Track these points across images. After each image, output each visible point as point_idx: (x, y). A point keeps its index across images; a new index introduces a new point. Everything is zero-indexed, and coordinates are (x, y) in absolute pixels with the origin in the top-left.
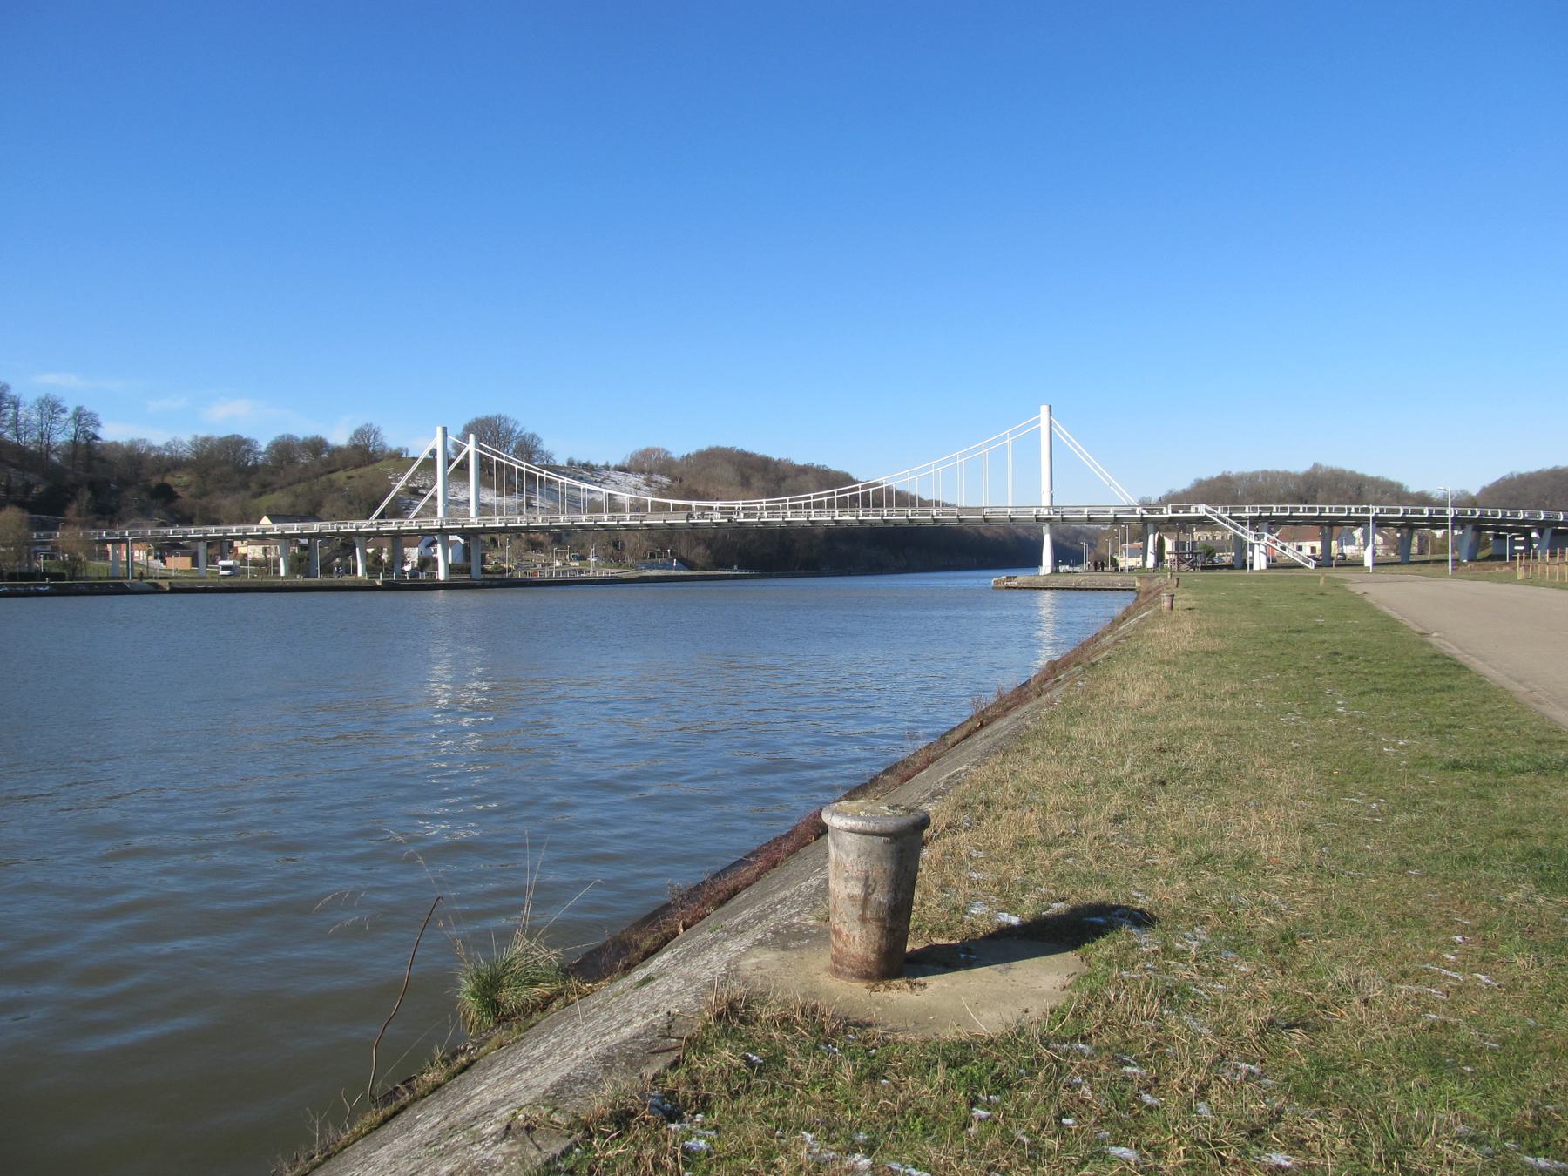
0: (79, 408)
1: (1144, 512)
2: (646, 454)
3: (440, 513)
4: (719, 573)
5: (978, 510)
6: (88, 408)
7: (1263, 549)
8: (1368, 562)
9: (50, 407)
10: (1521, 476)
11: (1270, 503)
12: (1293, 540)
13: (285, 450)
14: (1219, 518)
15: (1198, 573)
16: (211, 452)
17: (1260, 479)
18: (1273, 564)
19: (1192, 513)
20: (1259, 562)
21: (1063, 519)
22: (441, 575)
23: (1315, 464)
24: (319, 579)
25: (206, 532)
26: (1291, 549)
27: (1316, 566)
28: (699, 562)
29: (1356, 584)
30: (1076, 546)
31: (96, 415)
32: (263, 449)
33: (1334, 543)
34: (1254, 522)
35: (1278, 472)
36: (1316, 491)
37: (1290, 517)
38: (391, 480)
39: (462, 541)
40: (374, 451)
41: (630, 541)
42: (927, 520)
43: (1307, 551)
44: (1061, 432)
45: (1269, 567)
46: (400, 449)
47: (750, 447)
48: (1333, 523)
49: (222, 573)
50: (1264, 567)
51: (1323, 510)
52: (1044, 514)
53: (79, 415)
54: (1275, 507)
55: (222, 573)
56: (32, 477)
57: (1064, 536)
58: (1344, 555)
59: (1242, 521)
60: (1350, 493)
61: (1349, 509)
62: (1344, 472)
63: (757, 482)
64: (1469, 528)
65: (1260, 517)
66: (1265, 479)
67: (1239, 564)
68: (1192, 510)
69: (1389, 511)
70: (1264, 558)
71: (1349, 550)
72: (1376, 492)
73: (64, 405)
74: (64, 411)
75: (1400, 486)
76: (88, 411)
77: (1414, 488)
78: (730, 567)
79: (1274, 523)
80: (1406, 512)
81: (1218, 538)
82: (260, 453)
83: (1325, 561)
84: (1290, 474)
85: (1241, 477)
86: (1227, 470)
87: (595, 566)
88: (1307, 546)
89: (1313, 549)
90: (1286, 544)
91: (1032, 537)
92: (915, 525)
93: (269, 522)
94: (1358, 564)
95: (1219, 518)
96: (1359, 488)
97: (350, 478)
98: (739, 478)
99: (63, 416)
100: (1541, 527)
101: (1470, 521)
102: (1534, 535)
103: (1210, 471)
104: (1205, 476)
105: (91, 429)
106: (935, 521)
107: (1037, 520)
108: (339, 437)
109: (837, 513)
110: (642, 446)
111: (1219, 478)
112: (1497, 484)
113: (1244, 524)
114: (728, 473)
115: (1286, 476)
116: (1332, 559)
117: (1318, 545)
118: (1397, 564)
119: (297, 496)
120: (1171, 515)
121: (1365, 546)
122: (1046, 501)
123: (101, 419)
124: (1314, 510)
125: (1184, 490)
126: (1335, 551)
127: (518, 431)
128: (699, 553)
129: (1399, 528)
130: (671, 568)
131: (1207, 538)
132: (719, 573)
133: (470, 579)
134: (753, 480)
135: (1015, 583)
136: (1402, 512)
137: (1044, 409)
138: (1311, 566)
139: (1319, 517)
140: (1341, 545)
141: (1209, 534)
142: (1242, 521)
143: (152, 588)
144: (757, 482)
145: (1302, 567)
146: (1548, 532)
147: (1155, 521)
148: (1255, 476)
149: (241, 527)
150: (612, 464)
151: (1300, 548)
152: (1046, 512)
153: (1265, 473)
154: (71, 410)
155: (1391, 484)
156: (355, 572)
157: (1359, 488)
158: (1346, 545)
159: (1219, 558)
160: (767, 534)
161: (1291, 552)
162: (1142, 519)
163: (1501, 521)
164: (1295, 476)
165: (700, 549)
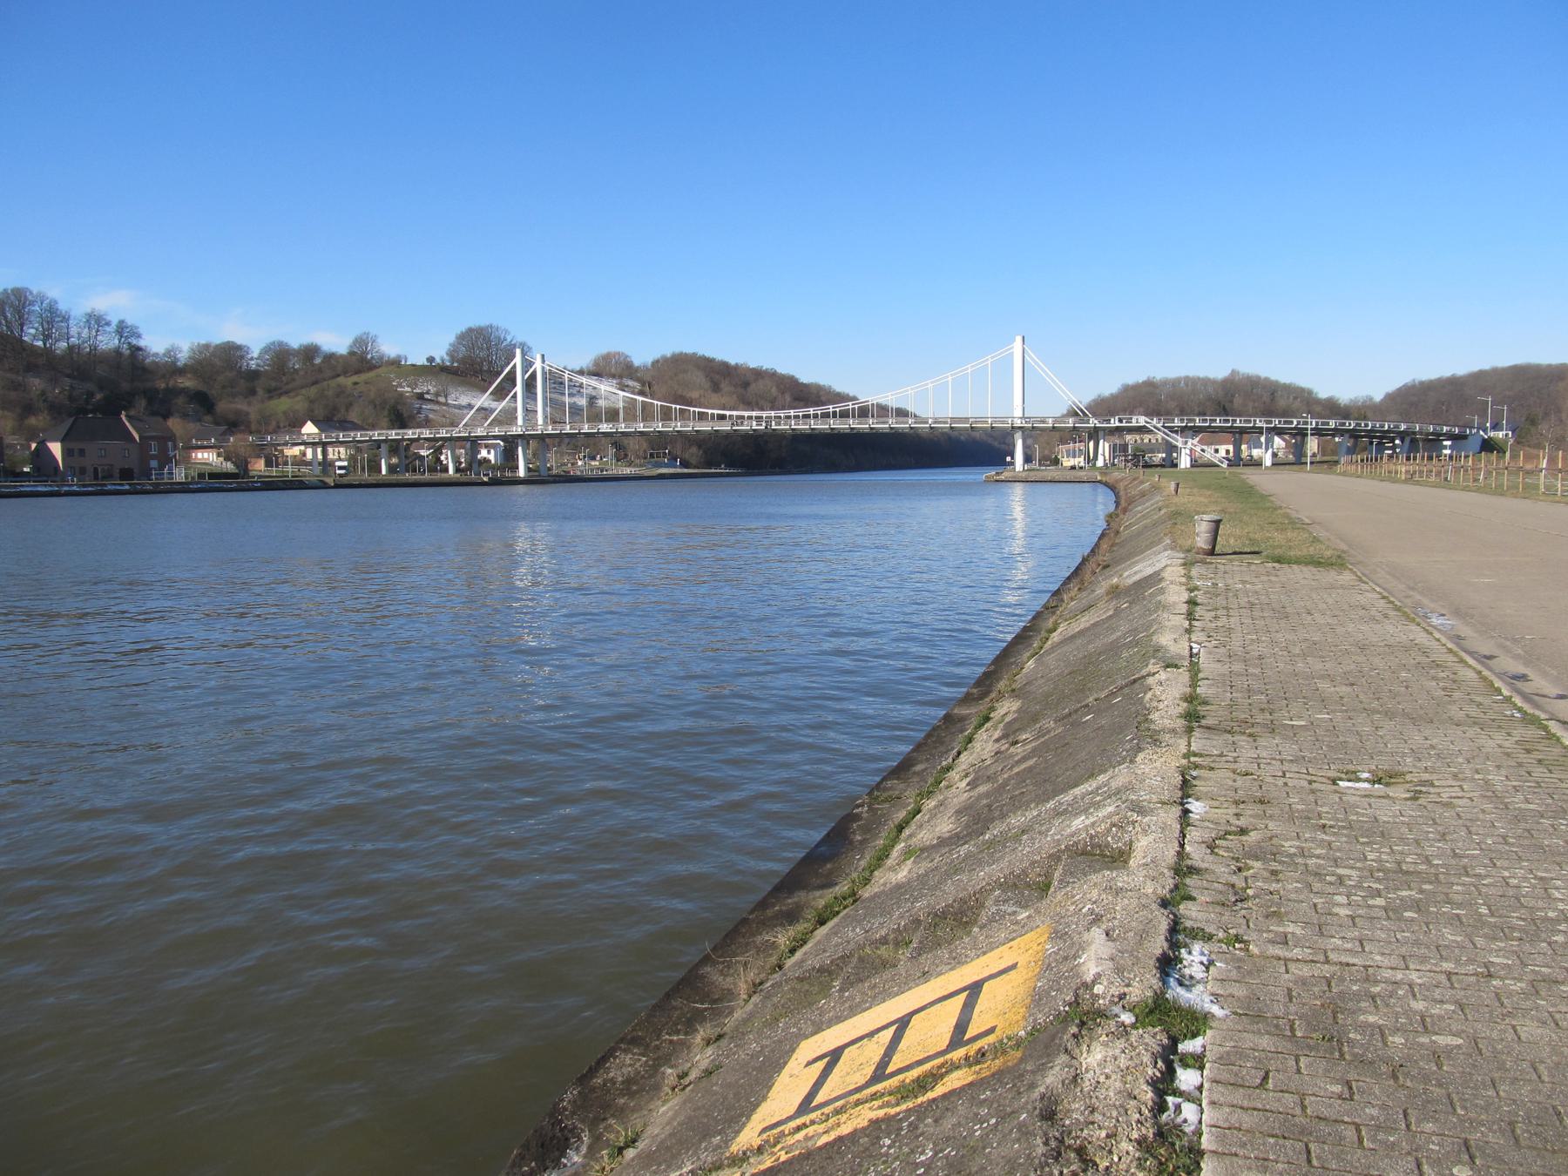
0: (121, 322)
1: (1096, 422)
2: (607, 358)
3: (520, 421)
4: (713, 471)
5: (966, 420)
6: (129, 322)
7: (1188, 452)
8: (1268, 461)
9: (96, 321)
10: (1422, 383)
11: (1194, 415)
12: (1212, 444)
13: (280, 355)
14: (1155, 427)
15: (1141, 470)
16: (213, 354)
17: (1182, 384)
18: (1195, 464)
19: (1134, 424)
20: (1184, 462)
21: (1033, 427)
22: (522, 472)
23: (1233, 371)
24: (427, 477)
25: (387, 435)
26: (1210, 450)
27: (1228, 465)
28: (693, 461)
29: (1251, 476)
30: (1003, 446)
31: (137, 328)
32: (255, 355)
33: (1244, 447)
34: (1183, 431)
35: (1199, 378)
36: (1233, 396)
37: (1209, 427)
38: (397, 386)
39: (502, 443)
40: (372, 358)
41: (632, 444)
42: (885, 428)
43: (1222, 453)
44: (1032, 357)
45: (1192, 466)
46: (399, 356)
47: (709, 354)
48: (1242, 431)
49: (338, 472)
50: (1188, 466)
51: (1234, 421)
52: (1018, 423)
53: (121, 329)
54: (1197, 419)
55: (338, 472)
56: (90, 386)
57: (991, 436)
58: (1252, 456)
59: (1171, 429)
60: (1265, 398)
61: (1255, 421)
62: (1259, 377)
63: (725, 386)
64: (1347, 435)
65: (1186, 426)
66: (1187, 385)
67: (1168, 463)
68: (1134, 421)
69: (1285, 422)
70: (1188, 459)
71: (1256, 453)
72: (1288, 398)
73: (108, 318)
74: (108, 324)
75: (1310, 392)
76: (129, 324)
77: (1323, 394)
78: (718, 466)
79: (1196, 431)
80: (1299, 423)
81: (1146, 441)
82: (252, 359)
83: (1236, 461)
84: (1209, 379)
85: (1165, 382)
86: (1152, 376)
87: (606, 463)
88: (1222, 449)
89: (1228, 452)
90: (1205, 447)
91: (962, 438)
92: (836, 432)
93: (316, 431)
94: (1258, 463)
95: (1155, 427)
96: (1272, 394)
97: (356, 383)
98: (709, 384)
99: (107, 329)
100: (1402, 435)
101: (1348, 431)
102: (1397, 442)
103: (1136, 376)
104: (1131, 381)
105: (134, 341)
106: (872, 429)
107: (1013, 428)
108: (336, 342)
109: (812, 422)
110: (604, 351)
111: (1145, 383)
112: (1399, 390)
113: (1176, 432)
114: (699, 378)
115: (1206, 382)
116: (1242, 460)
117: (1231, 448)
118: (1293, 464)
119: (312, 402)
120: (1117, 424)
121: (1267, 449)
122: (1018, 413)
123: (141, 331)
124: (1228, 421)
125: (1112, 394)
126: (1245, 454)
127: (509, 340)
128: (693, 453)
129: (1294, 436)
130: (675, 467)
131: (1136, 441)
132: (713, 471)
133: (540, 476)
134: (722, 386)
135: (1002, 477)
136: (1295, 423)
137: (1019, 339)
138: (1225, 466)
139: (1231, 427)
140: (1249, 448)
141: (1138, 437)
142: (1171, 429)
143: (320, 484)
144: (725, 386)
145: (1218, 466)
146: (1407, 440)
147: (1104, 429)
148: (1178, 380)
149: (401, 431)
150: (570, 368)
151: (1217, 451)
152: (1019, 421)
153: (1187, 378)
154: (115, 322)
155: (1302, 390)
156: (446, 470)
157: (1272, 394)
158: (1255, 448)
159: (1150, 458)
160: (755, 439)
161: (1209, 454)
162: (1095, 427)
163: (1388, 431)
164: (1214, 382)
165: (694, 450)
